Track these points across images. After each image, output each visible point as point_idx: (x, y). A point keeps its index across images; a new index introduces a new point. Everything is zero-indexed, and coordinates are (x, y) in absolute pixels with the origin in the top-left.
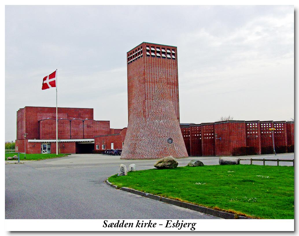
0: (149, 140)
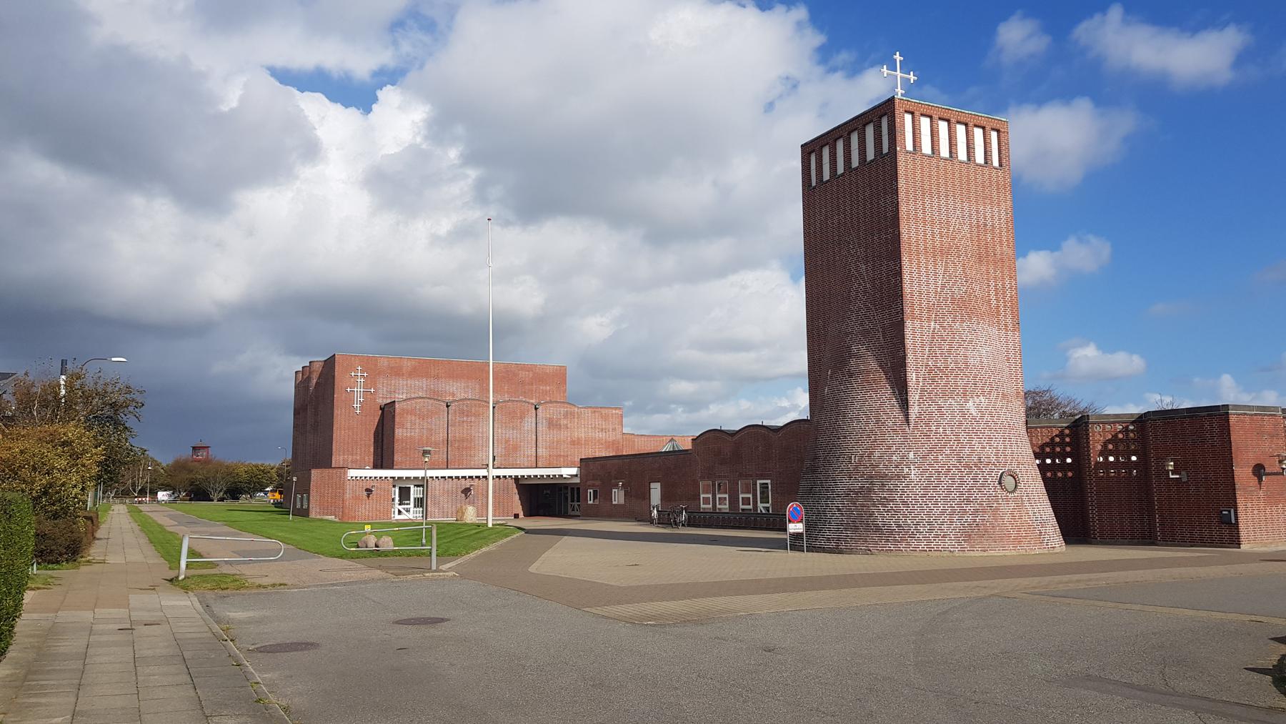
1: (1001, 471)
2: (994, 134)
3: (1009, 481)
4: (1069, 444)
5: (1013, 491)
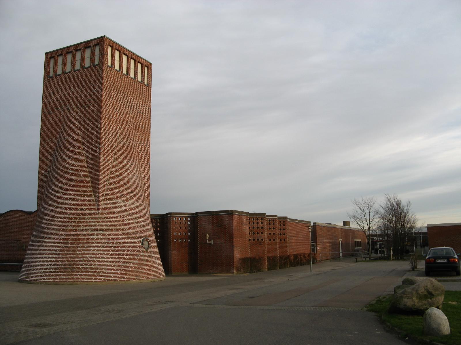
0: (108, 242)
1: (142, 238)
2: (146, 68)
3: (146, 243)
4: (159, 227)
5: (147, 249)
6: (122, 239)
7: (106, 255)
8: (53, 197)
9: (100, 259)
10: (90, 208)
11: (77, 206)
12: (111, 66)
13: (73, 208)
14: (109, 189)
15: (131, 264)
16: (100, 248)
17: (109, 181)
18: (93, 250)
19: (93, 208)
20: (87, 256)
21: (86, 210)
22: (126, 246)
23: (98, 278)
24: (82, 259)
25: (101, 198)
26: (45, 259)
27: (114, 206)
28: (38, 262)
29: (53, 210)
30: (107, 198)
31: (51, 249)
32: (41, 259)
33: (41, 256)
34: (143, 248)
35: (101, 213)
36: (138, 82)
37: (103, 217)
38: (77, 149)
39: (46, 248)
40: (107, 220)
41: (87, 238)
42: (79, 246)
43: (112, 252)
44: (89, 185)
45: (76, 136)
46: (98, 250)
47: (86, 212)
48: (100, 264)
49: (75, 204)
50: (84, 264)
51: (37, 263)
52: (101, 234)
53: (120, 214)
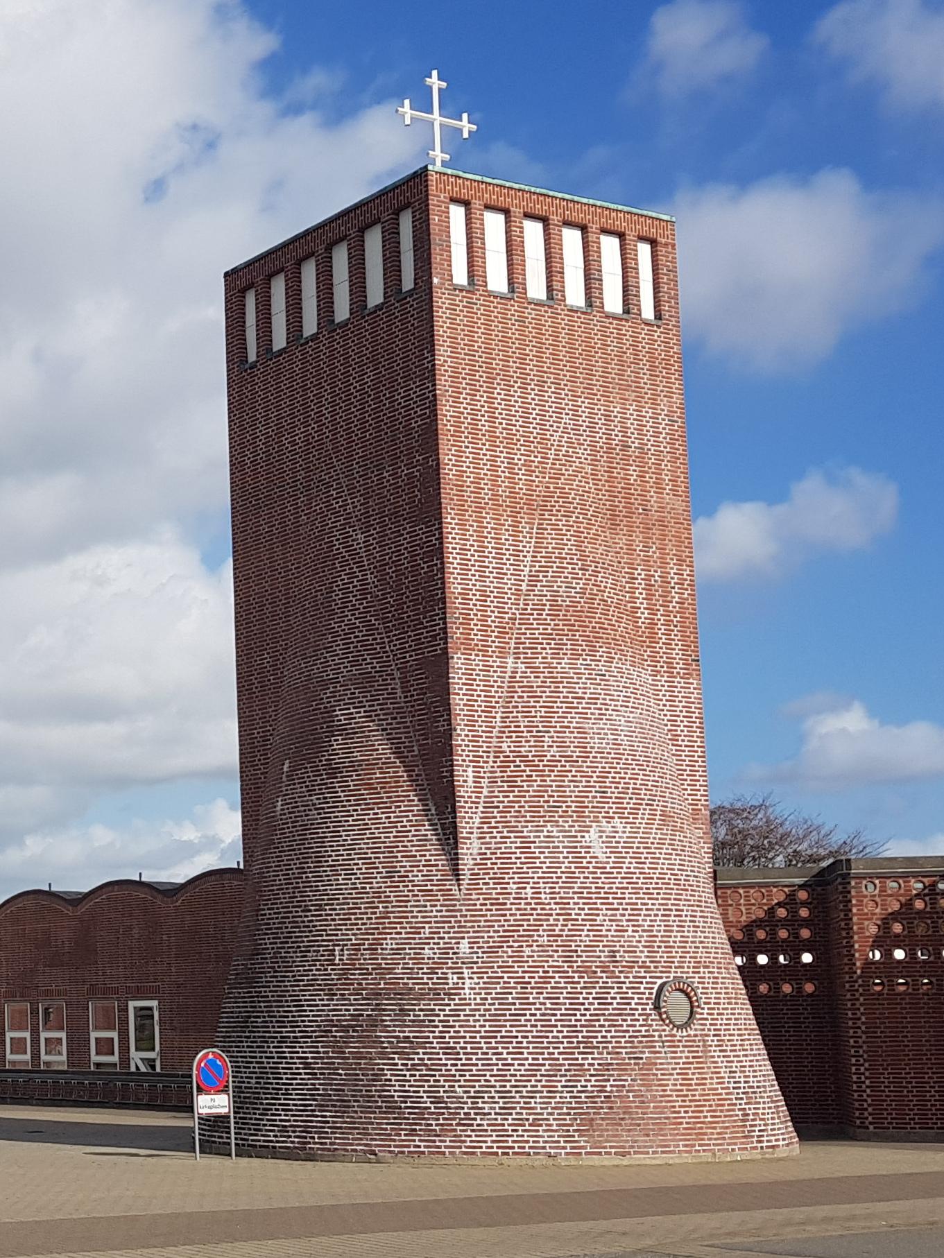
1: (659, 982)
2: (644, 250)
3: (676, 1004)
6: (563, 985)
7: (497, 1048)
8: (288, 828)
9: (473, 1065)
10: (424, 866)
11: (375, 858)
12: (469, 284)
13: (361, 869)
14: (500, 784)
15: (608, 1089)
16: (469, 1021)
17: (495, 752)
18: (441, 1029)
19: (437, 865)
20: (418, 1053)
21: (410, 874)
22: (581, 1015)
23: (465, 1141)
24: (402, 1065)
25: (468, 823)
26: (268, 1063)
27: (521, 853)
28: (245, 1073)
29: (290, 879)
30: (493, 820)
31: (369, 819)
32: (257, 1063)
33: (255, 1052)
34: (663, 1020)
35: (469, 884)
36: (607, 317)
37: (479, 899)
38: (363, 636)
39: (272, 1022)
40: (497, 910)
41: (418, 984)
42: (389, 1015)
43: (522, 1037)
44: (417, 775)
45: (356, 586)
46: (462, 1029)
47: (409, 881)
48: (474, 1087)
49: (367, 853)
50: (410, 1086)
51: (242, 1077)
52: (472, 968)
53: (553, 883)
